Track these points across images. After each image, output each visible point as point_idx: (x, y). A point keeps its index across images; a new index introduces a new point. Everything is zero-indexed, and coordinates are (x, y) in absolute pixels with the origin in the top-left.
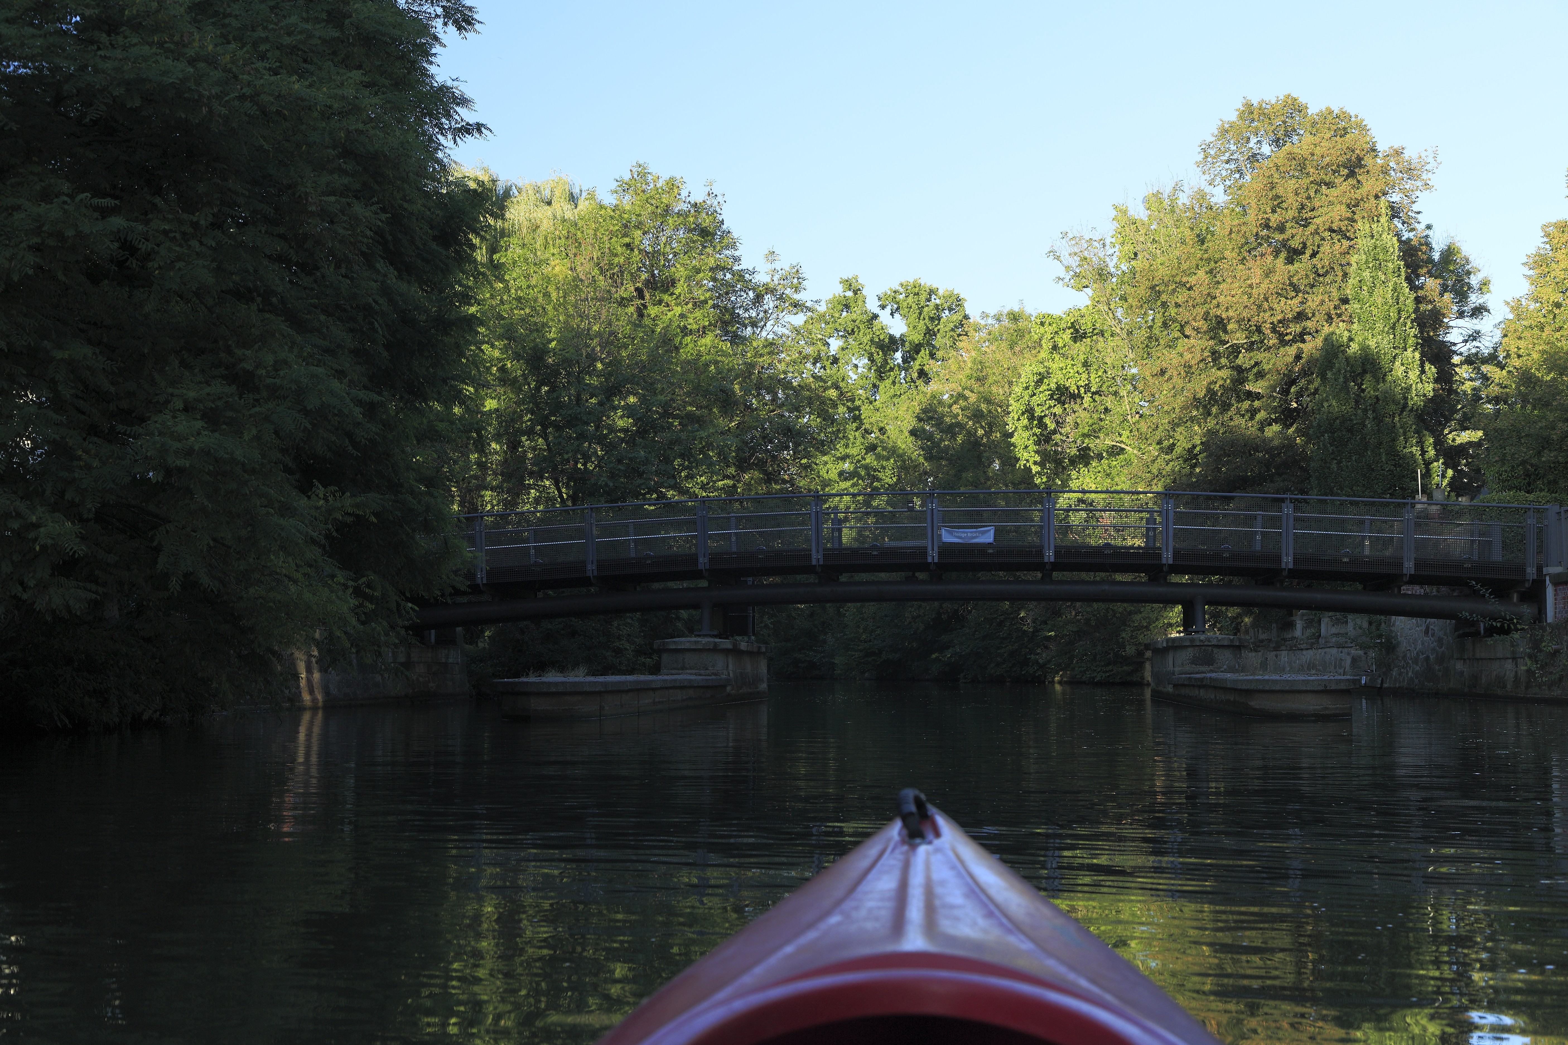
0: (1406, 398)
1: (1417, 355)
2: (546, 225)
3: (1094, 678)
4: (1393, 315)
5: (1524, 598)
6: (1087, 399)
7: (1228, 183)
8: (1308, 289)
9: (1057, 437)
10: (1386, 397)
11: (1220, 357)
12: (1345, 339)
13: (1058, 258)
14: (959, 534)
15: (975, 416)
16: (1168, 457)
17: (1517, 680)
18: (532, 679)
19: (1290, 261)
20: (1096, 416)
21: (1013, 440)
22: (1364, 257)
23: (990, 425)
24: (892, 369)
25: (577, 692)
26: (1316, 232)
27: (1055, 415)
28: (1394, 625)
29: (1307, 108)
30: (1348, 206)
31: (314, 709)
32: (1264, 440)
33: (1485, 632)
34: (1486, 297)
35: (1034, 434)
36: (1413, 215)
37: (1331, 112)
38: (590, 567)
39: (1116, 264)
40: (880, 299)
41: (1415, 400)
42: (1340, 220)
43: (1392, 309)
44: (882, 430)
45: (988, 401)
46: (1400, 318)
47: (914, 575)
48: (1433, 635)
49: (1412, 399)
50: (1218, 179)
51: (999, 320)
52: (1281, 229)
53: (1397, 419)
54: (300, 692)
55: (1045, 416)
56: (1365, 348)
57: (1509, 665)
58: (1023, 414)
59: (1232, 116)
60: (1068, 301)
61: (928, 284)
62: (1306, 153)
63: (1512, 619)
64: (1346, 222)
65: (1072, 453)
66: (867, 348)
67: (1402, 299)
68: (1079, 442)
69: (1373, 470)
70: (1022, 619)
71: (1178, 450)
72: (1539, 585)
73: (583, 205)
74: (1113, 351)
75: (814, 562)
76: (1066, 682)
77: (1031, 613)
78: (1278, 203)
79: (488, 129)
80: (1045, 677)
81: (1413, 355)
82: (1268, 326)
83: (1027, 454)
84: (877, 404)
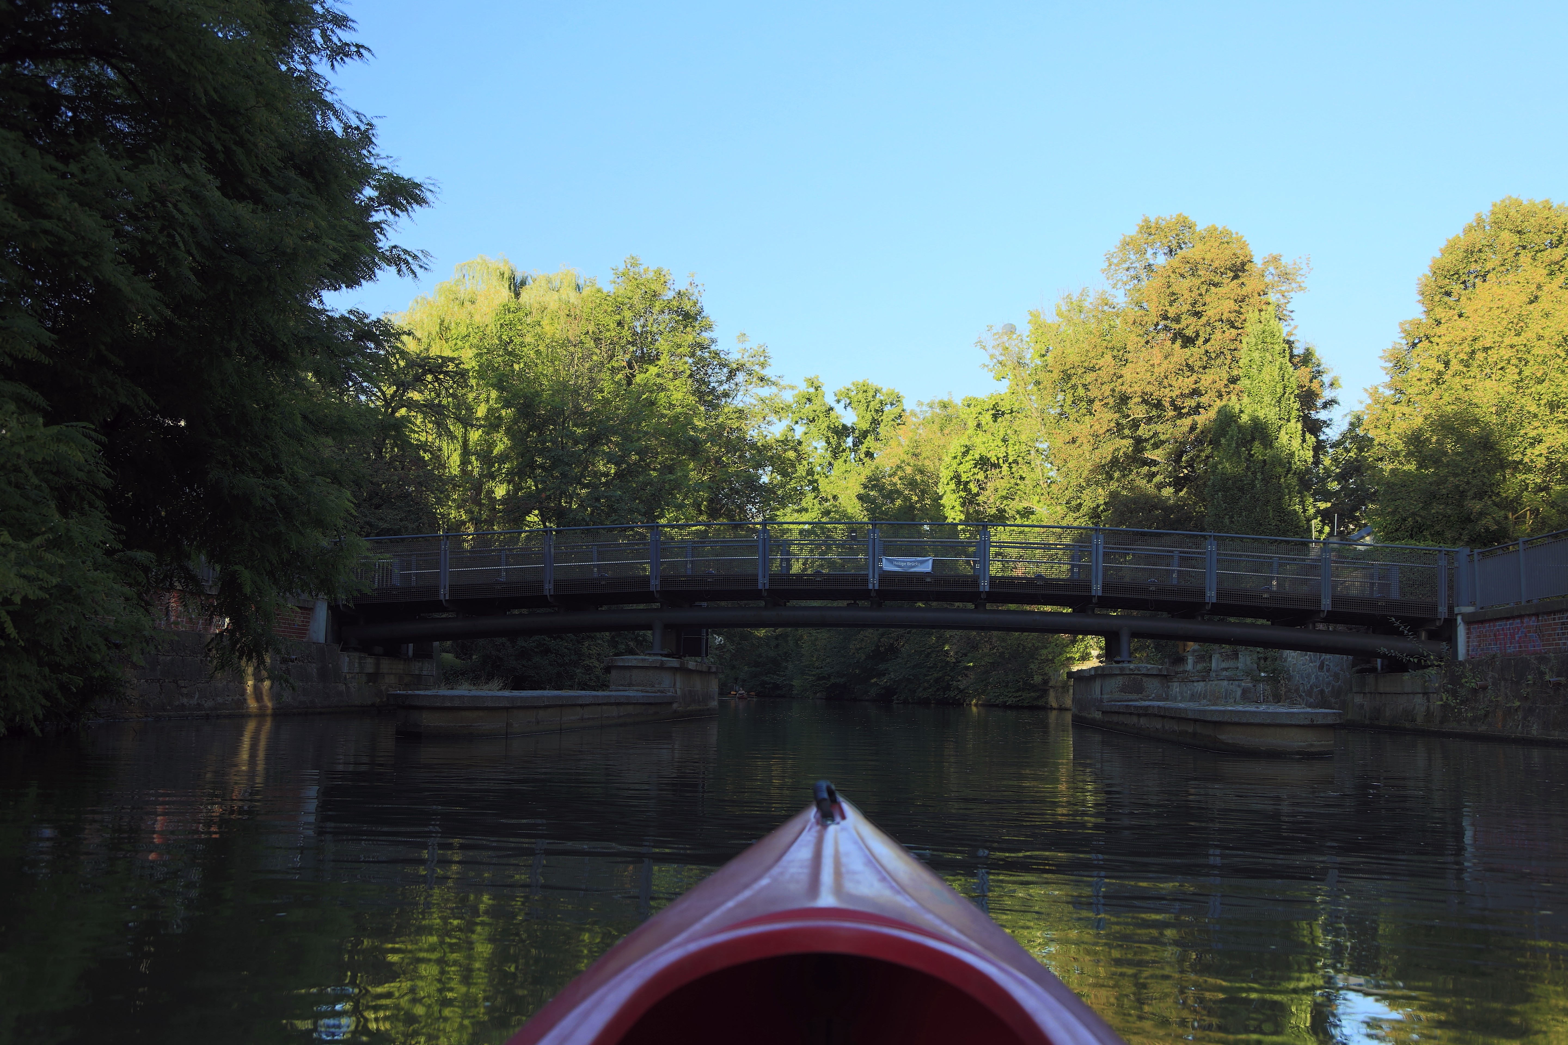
0: (1290, 463)
1: (1299, 426)
2: (553, 306)
3: (1006, 702)
4: (1280, 390)
5: (1434, 636)
6: (1005, 467)
7: (1128, 287)
8: (1201, 370)
9: (981, 499)
10: (1273, 461)
11: (1124, 429)
12: (1237, 411)
13: (984, 348)
14: (900, 564)
15: (910, 484)
16: (1077, 514)
17: (1429, 715)
18: (444, 692)
19: (1184, 346)
20: (1013, 481)
21: (942, 502)
22: (1254, 340)
23: (923, 492)
24: (844, 450)
25: (476, 706)
26: (1208, 324)
27: (978, 481)
28: (1285, 661)
29: (1195, 225)
30: (1236, 301)
31: (261, 716)
32: (1160, 500)
33: (1382, 669)
34: (1338, 391)
35: (961, 497)
36: (1288, 313)
37: (1216, 229)
38: (547, 586)
39: (1031, 357)
40: (836, 395)
41: (1297, 464)
42: (1230, 312)
43: (1278, 386)
44: (835, 497)
45: (922, 472)
46: (1285, 393)
47: (855, 603)
48: (1328, 670)
49: (1295, 463)
50: (1120, 283)
51: (931, 407)
52: (1177, 320)
53: (1282, 480)
54: (245, 700)
55: (971, 481)
56: (1255, 420)
57: (1419, 700)
58: (951, 479)
59: (1132, 230)
60: (990, 387)
61: (875, 384)
62: (1198, 258)
63: (1429, 655)
64: (1234, 314)
65: (992, 513)
66: (825, 432)
67: (1287, 376)
68: (998, 503)
69: (1261, 525)
70: (947, 652)
71: (1084, 509)
72: (1451, 623)
73: (586, 292)
74: (1028, 429)
75: (760, 587)
76: (982, 705)
77: (955, 647)
78: (1174, 298)
79: (353, 21)
80: (964, 701)
81: (1296, 426)
82: (1168, 399)
83: (954, 513)
84: (832, 478)
